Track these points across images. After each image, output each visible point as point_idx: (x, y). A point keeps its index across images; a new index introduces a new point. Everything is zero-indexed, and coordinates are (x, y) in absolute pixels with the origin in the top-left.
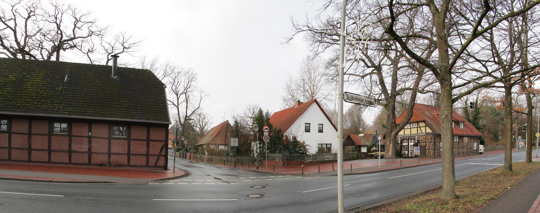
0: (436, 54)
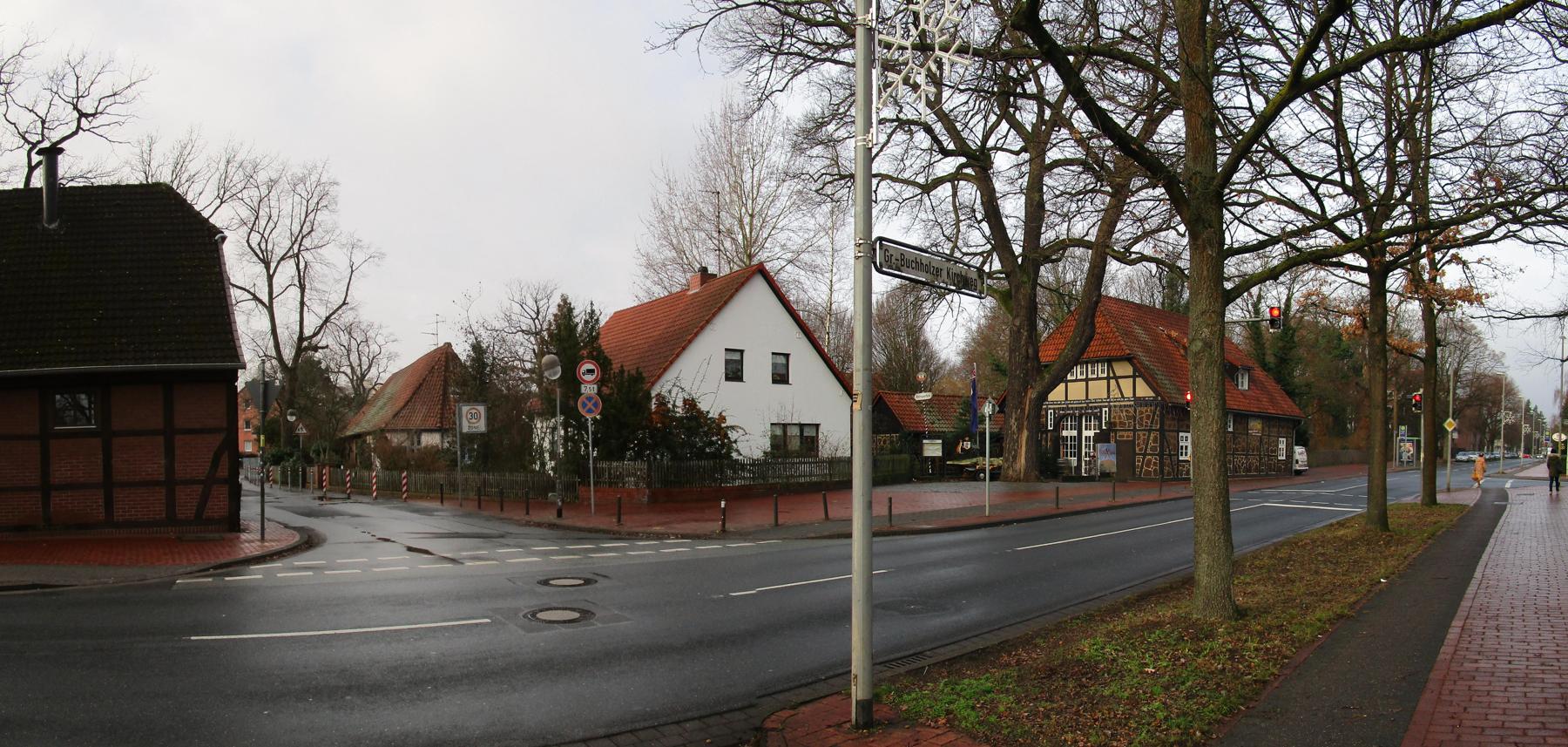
0: (1173, 127)
